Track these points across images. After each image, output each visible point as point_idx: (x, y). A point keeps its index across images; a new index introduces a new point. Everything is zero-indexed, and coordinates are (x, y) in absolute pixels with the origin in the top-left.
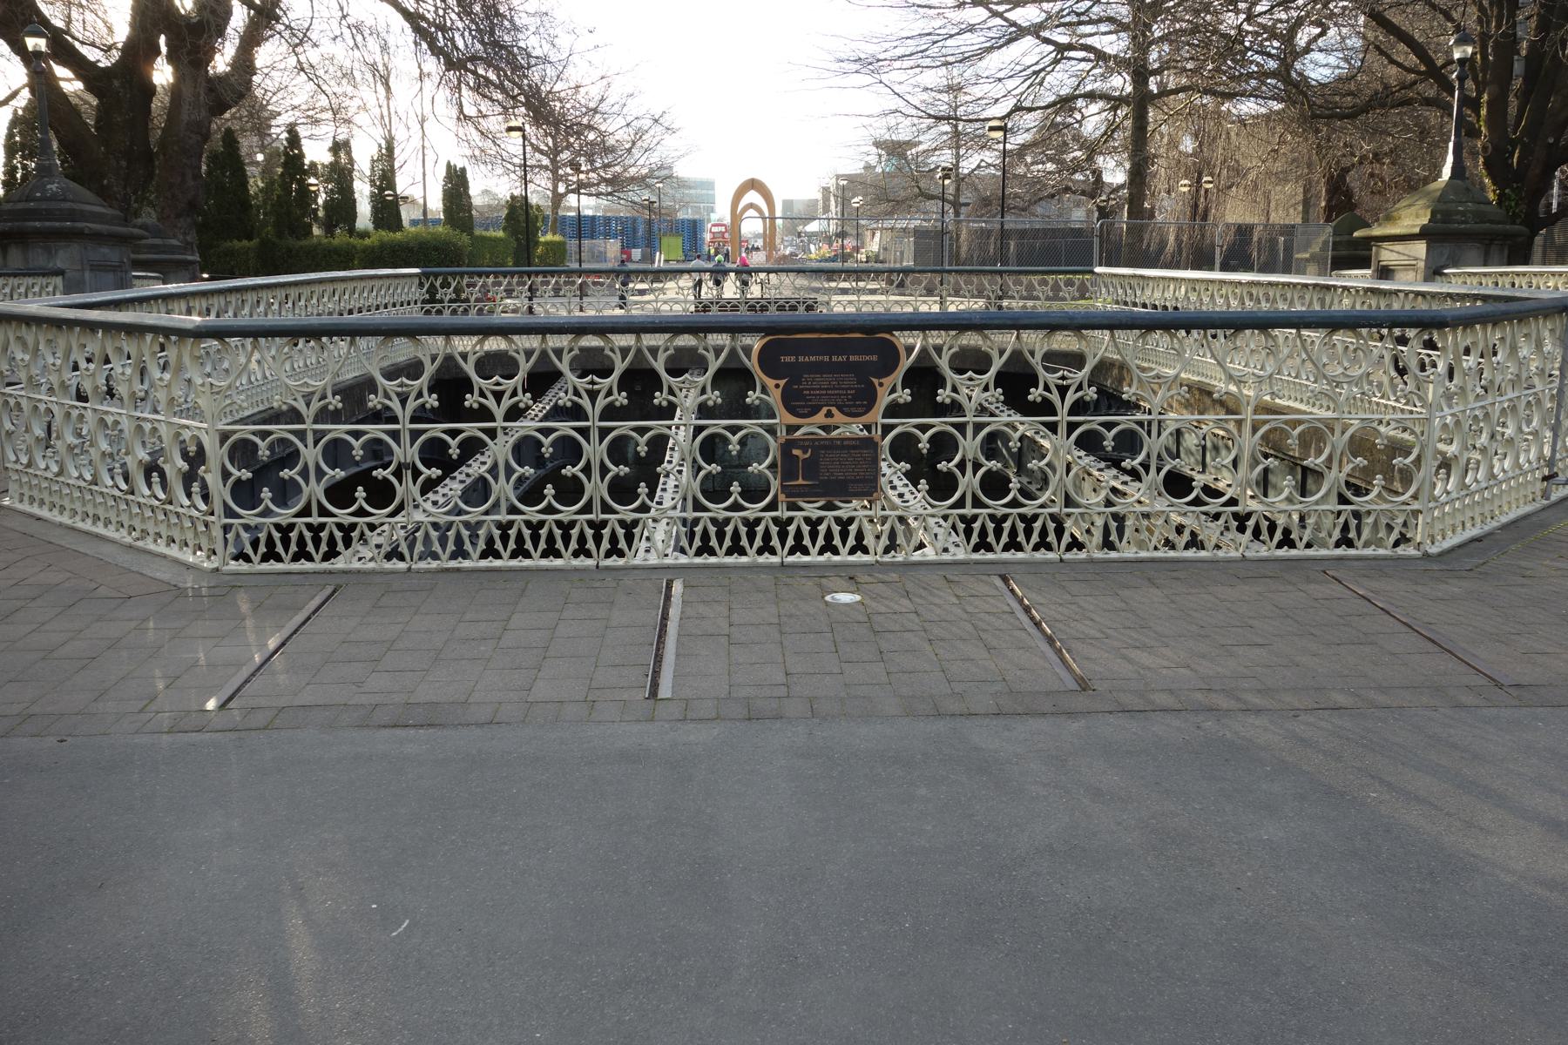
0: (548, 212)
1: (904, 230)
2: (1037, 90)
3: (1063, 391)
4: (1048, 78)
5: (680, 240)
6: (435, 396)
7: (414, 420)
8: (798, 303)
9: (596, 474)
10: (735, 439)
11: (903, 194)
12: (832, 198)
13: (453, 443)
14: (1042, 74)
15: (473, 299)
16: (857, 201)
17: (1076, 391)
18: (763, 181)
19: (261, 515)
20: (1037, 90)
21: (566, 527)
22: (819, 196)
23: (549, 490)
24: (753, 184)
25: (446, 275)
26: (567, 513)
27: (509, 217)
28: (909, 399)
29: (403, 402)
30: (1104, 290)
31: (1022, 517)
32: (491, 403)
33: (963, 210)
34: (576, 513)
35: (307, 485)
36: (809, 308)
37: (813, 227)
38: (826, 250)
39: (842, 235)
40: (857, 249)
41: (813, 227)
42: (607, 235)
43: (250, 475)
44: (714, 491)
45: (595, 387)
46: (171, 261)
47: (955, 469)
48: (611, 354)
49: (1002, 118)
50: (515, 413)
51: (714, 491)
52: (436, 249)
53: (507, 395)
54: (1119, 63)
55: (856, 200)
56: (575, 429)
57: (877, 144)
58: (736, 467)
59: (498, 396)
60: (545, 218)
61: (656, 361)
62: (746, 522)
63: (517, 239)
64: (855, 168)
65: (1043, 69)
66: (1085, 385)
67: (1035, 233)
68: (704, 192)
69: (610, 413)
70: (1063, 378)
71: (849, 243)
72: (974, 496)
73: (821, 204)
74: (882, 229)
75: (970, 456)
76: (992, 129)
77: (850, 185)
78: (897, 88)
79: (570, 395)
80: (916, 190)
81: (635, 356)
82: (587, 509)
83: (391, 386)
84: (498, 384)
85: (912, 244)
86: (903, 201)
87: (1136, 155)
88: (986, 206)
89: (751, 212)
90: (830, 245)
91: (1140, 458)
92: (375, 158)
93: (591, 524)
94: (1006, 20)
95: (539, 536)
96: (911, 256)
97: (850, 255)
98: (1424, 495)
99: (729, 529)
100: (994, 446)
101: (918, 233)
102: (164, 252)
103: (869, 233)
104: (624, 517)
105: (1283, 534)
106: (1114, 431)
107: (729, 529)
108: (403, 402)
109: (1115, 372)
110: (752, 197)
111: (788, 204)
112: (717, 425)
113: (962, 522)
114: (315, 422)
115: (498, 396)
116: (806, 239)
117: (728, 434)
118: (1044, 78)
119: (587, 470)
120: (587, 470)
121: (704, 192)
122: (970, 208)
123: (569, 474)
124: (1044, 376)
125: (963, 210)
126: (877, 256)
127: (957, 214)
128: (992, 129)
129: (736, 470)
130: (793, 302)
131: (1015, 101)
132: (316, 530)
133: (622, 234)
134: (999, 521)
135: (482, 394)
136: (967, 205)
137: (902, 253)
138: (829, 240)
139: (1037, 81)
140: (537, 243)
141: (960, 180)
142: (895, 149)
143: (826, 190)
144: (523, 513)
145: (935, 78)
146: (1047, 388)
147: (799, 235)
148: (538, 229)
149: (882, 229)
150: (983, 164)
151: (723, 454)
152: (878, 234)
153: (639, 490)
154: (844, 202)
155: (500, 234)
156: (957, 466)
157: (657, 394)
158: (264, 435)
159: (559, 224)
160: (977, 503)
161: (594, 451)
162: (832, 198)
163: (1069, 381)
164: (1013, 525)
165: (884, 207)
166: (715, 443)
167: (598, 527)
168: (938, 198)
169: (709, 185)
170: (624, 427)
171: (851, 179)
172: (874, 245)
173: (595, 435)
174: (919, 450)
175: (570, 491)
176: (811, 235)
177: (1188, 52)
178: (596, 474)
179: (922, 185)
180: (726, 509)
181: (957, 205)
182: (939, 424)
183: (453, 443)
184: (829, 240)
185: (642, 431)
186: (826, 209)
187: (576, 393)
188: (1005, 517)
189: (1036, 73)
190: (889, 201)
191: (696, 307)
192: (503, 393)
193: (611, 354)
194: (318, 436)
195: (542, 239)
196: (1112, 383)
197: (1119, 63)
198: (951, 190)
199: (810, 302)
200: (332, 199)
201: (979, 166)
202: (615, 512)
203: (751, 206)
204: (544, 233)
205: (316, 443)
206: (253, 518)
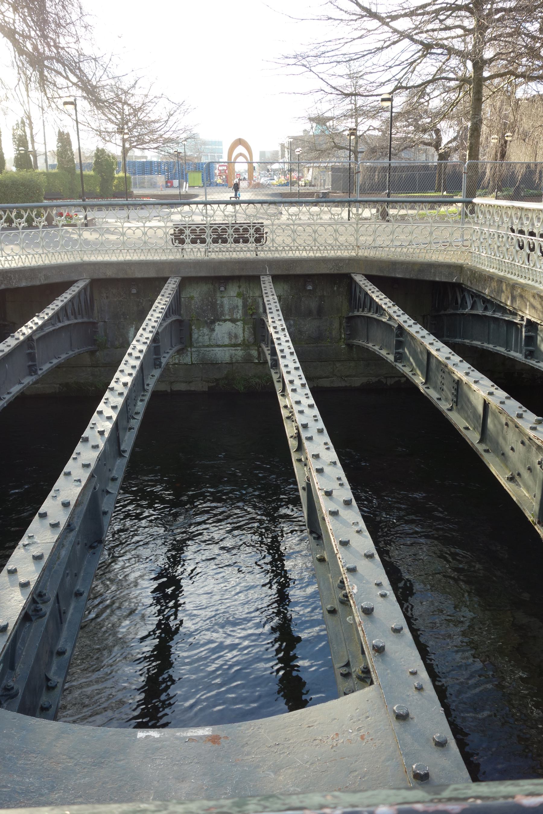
0: (121, 160)
1: (326, 167)
2: (410, 76)
4: (418, 68)
5: (200, 174)
8: (185, 227)
9: (231, 237)
11: (324, 147)
12: (286, 150)
14: (414, 65)
15: (20, 227)
16: (298, 151)
20: (410, 76)
22: (279, 148)
24: (240, 142)
27: (96, 163)
30: (481, 216)
33: (360, 155)
36: (75, 459)
37: (276, 166)
38: (283, 180)
39: (291, 171)
40: (299, 179)
41: (276, 166)
42: (159, 172)
44: (192, 364)
49: (390, 94)
51: (192, 364)
52: (23, 185)
54: (463, 55)
55: (298, 150)
57: (311, 119)
58: (208, 346)
60: (118, 164)
63: (102, 176)
64: (299, 133)
65: (415, 61)
67: (403, 169)
68: (217, 147)
71: (295, 175)
73: (280, 153)
74: (313, 167)
76: (383, 100)
77: (296, 141)
78: (321, 76)
80: (333, 144)
85: (330, 176)
86: (325, 151)
87: (474, 118)
88: (373, 153)
89: (241, 159)
90: (285, 176)
92: (15, 128)
94: (391, 27)
96: (330, 183)
97: (295, 182)
100: (401, 351)
101: (333, 169)
103: (306, 169)
109: (494, 284)
110: (240, 149)
111: (262, 154)
116: (272, 173)
118: (415, 68)
121: (217, 147)
122: (364, 154)
125: (360, 155)
126: (310, 182)
127: (356, 158)
128: (383, 100)
129: (208, 349)
130: (245, 226)
131: (396, 83)
133: (168, 172)
136: (362, 152)
137: (325, 181)
138: (284, 173)
139: (410, 70)
140: (113, 178)
141: (358, 138)
142: (320, 120)
143: (283, 146)
145: (342, 69)
147: (268, 171)
148: (113, 170)
149: (313, 167)
150: (371, 128)
151: (198, 338)
152: (311, 170)
154: (292, 152)
155: (92, 173)
159: (126, 165)
162: (286, 150)
165: (313, 154)
166: (191, 330)
168: (347, 149)
169: (220, 143)
171: (295, 138)
172: (309, 176)
173: (230, 228)
176: (275, 171)
178: (231, 237)
179: (336, 141)
181: (356, 153)
184: (284, 173)
186: (283, 156)
189: (412, 63)
190: (317, 151)
191: (175, 230)
195: (116, 176)
196: (492, 292)
197: (463, 55)
198: (353, 143)
199: (258, 226)
200: (20, 154)
201: (368, 130)
203: (241, 154)
204: (118, 172)
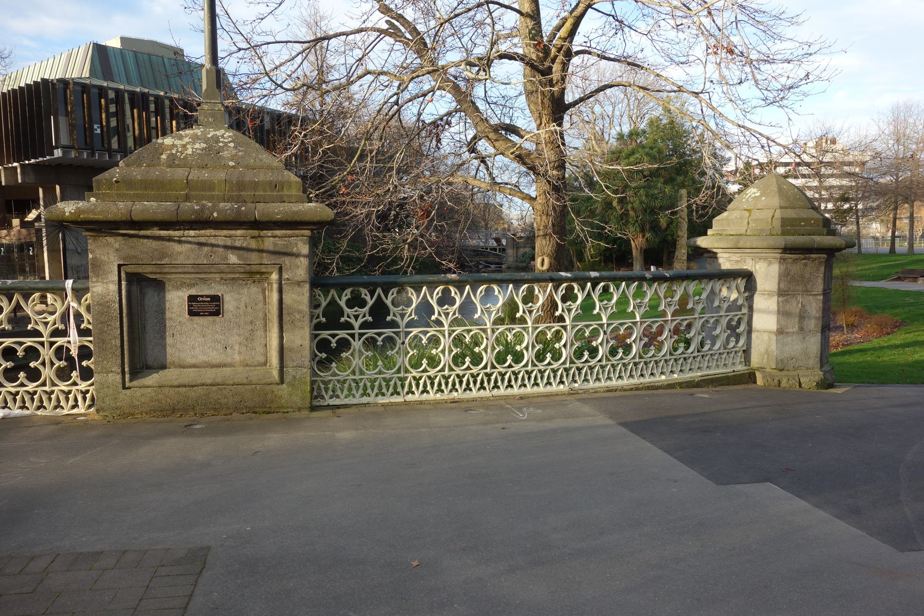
7: (360, 328)
9: (357, 355)
10: (380, 339)
21: (387, 381)
26: (31, 387)
31: (385, 379)
32: (352, 321)
34: (393, 374)
45: (404, 312)
48: (365, 297)
53: (535, 311)
59: (356, 317)
69: (364, 325)
75: (357, 348)
82: (44, 384)
83: (37, 318)
84: (356, 311)
95: (374, 386)
112: (325, 334)
115: (356, 317)
135: (348, 317)
144: (321, 377)
146: (394, 315)
161: (445, 342)
170: (371, 332)
175: (34, 375)
177: (409, 188)
178: (357, 355)
182: (29, 342)
183: (334, 341)
185: (334, 336)
192: (533, 311)
193: (365, 297)
205: (360, 339)
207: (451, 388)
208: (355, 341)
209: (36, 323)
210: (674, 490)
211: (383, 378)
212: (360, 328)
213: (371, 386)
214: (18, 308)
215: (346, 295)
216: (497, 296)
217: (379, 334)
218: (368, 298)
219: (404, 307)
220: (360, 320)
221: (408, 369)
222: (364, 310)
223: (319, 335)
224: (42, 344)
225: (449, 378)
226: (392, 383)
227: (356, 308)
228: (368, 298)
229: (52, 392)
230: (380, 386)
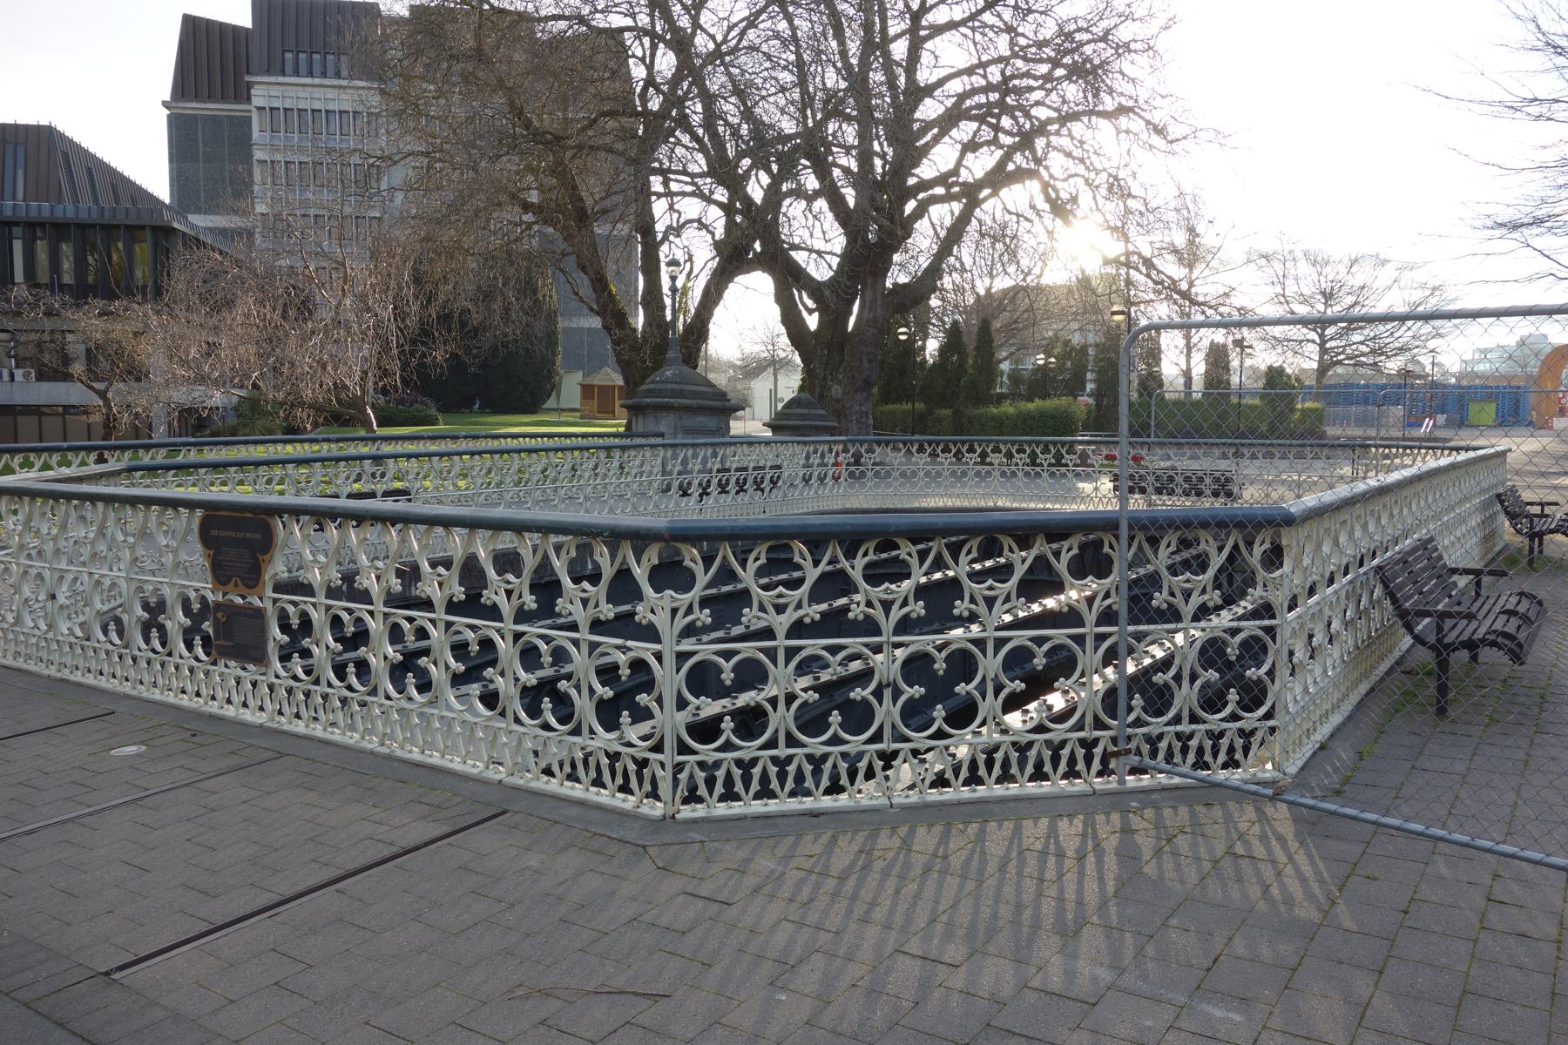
3: (1187, 595)
6: (921, 603)
13: (727, 666)
17: (1004, 603)
18: (773, 299)
19: (827, 743)
23: (835, 718)
25: (998, 442)
28: (923, 612)
29: (887, 611)
35: (775, 710)
43: (957, 689)
46: (811, 426)
47: (871, 698)
50: (1203, 612)
52: (1053, 417)
53: (895, 607)
56: (761, 650)
59: (887, 606)
61: (745, 571)
62: (739, 763)
66: (1209, 588)
70: (991, 588)
72: (1096, 718)
79: (862, 607)
81: (935, 558)
82: (771, 744)
91: (1265, 668)
93: (1082, 742)
98: (1279, 713)
99: (720, 774)
102: (808, 420)
104: (1214, 727)
105: (830, 779)
106: (1046, 647)
107: (720, 774)
108: (887, 611)
113: (774, 764)
114: (788, 637)
117: (721, 660)
119: (982, 689)
120: (982, 689)
123: (859, 698)
124: (970, 588)
130: (1200, 474)
132: (782, 764)
134: (1216, 737)
144: (804, 746)
153: (831, 719)
155: (1257, 402)
156: (872, 693)
157: (958, 603)
158: (727, 655)
160: (792, 742)
163: (894, 596)
164: (765, 771)
167: (782, 764)
174: (722, 682)
180: (717, 750)
183: (727, 666)
187: (869, 604)
188: (825, 757)
192: (892, 602)
193: (692, 565)
194: (682, 657)
202: (694, 752)
206: (927, 741)
207: (1226, 758)
208: (985, 657)
209: (973, 600)
210: (1149, 1023)
211: (1046, 741)
212: (896, 632)
213: (742, 776)
214: (727, 574)
215: (757, 559)
216: (1107, 555)
217: (834, 650)
218: (698, 569)
219: (784, 590)
220: (896, 614)
221: (1173, 718)
222: (687, 596)
223: (800, 649)
224: (1080, 640)
225: (1096, 746)
226: (1065, 752)
227: (1188, 574)
228: (698, 569)
229: (790, 759)
230: (765, 777)
